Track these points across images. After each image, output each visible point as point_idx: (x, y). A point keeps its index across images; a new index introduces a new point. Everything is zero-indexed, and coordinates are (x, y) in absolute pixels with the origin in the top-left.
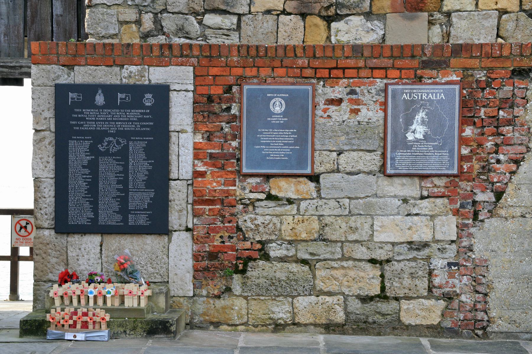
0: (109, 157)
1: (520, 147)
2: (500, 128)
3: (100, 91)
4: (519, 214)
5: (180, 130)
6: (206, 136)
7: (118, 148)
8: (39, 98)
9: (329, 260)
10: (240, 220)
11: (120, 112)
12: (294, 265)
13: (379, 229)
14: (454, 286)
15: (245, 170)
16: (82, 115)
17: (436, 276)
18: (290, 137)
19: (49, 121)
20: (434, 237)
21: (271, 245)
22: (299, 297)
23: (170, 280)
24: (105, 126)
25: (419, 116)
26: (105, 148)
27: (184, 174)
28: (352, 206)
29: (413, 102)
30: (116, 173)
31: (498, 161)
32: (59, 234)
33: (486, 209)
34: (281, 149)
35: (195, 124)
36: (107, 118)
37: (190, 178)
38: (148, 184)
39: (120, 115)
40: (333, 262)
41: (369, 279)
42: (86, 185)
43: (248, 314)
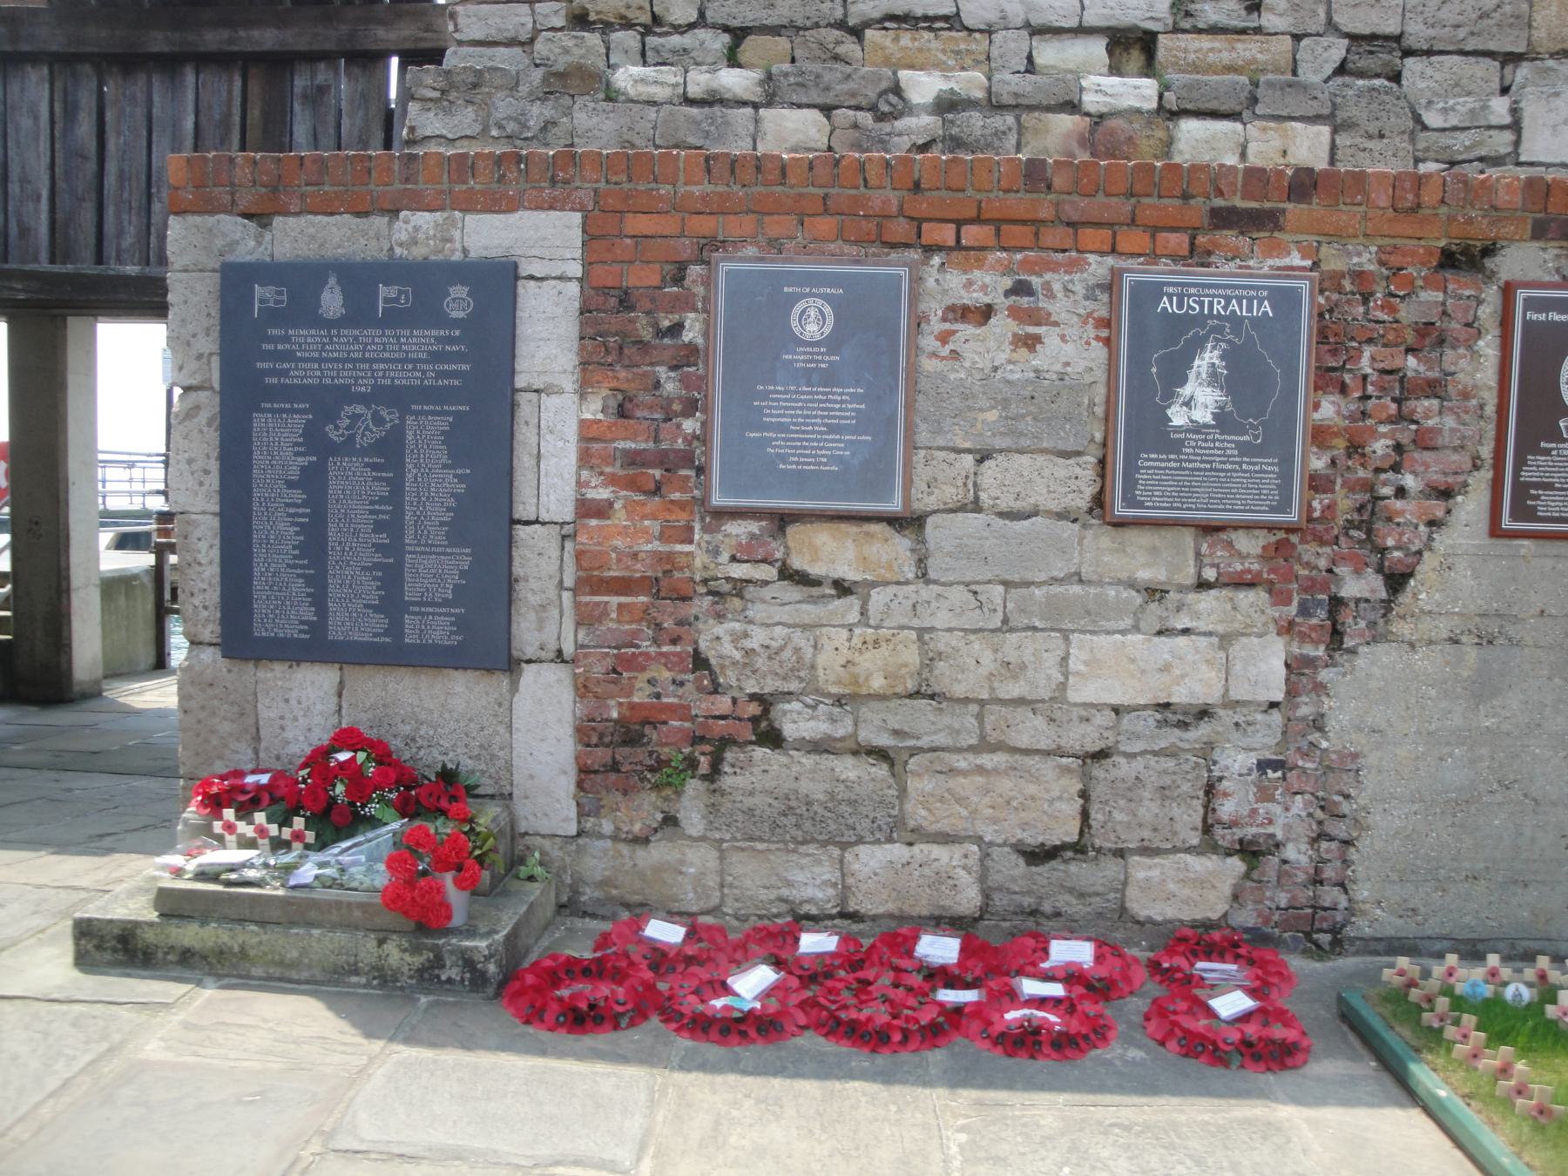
0: (354, 459)
1: (1455, 457)
2: (1408, 403)
3: (332, 281)
4: (1445, 634)
5: (542, 387)
6: (613, 404)
7: (378, 433)
8: (186, 302)
9: (943, 750)
10: (703, 636)
11: (383, 335)
12: (849, 760)
13: (1082, 668)
14: (1271, 822)
15: (717, 500)
16: (287, 346)
17: (1226, 795)
18: (846, 410)
19: (209, 363)
20: (1227, 690)
21: (787, 706)
22: (861, 847)
23: (516, 792)
24: (346, 374)
25: (1203, 359)
26: (342, 435)
27: (553, 507)
28: (1010, 605)
29: (1186, 321)
30: (372, 503)
31: (1401, 492)
32: (515, 595)
33: (1363, 619)
34: (819, 441)
35: (583, 370)
36: (349, 352)
37: (569, 518)
38: (457, 533)
39: (384, 344)
40: (955, 757)
41: (1051, 802)
42: (297, 534)
43: (722, 886)
